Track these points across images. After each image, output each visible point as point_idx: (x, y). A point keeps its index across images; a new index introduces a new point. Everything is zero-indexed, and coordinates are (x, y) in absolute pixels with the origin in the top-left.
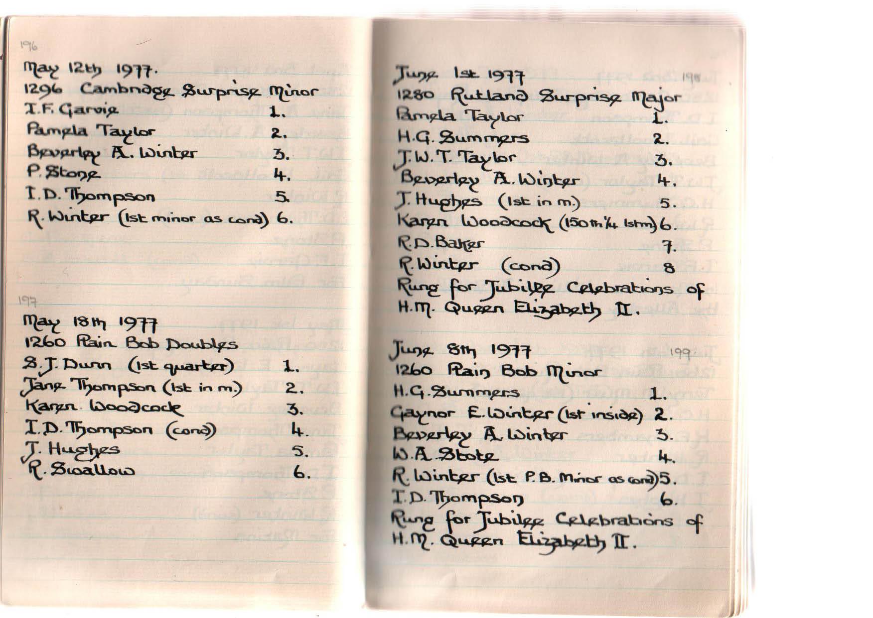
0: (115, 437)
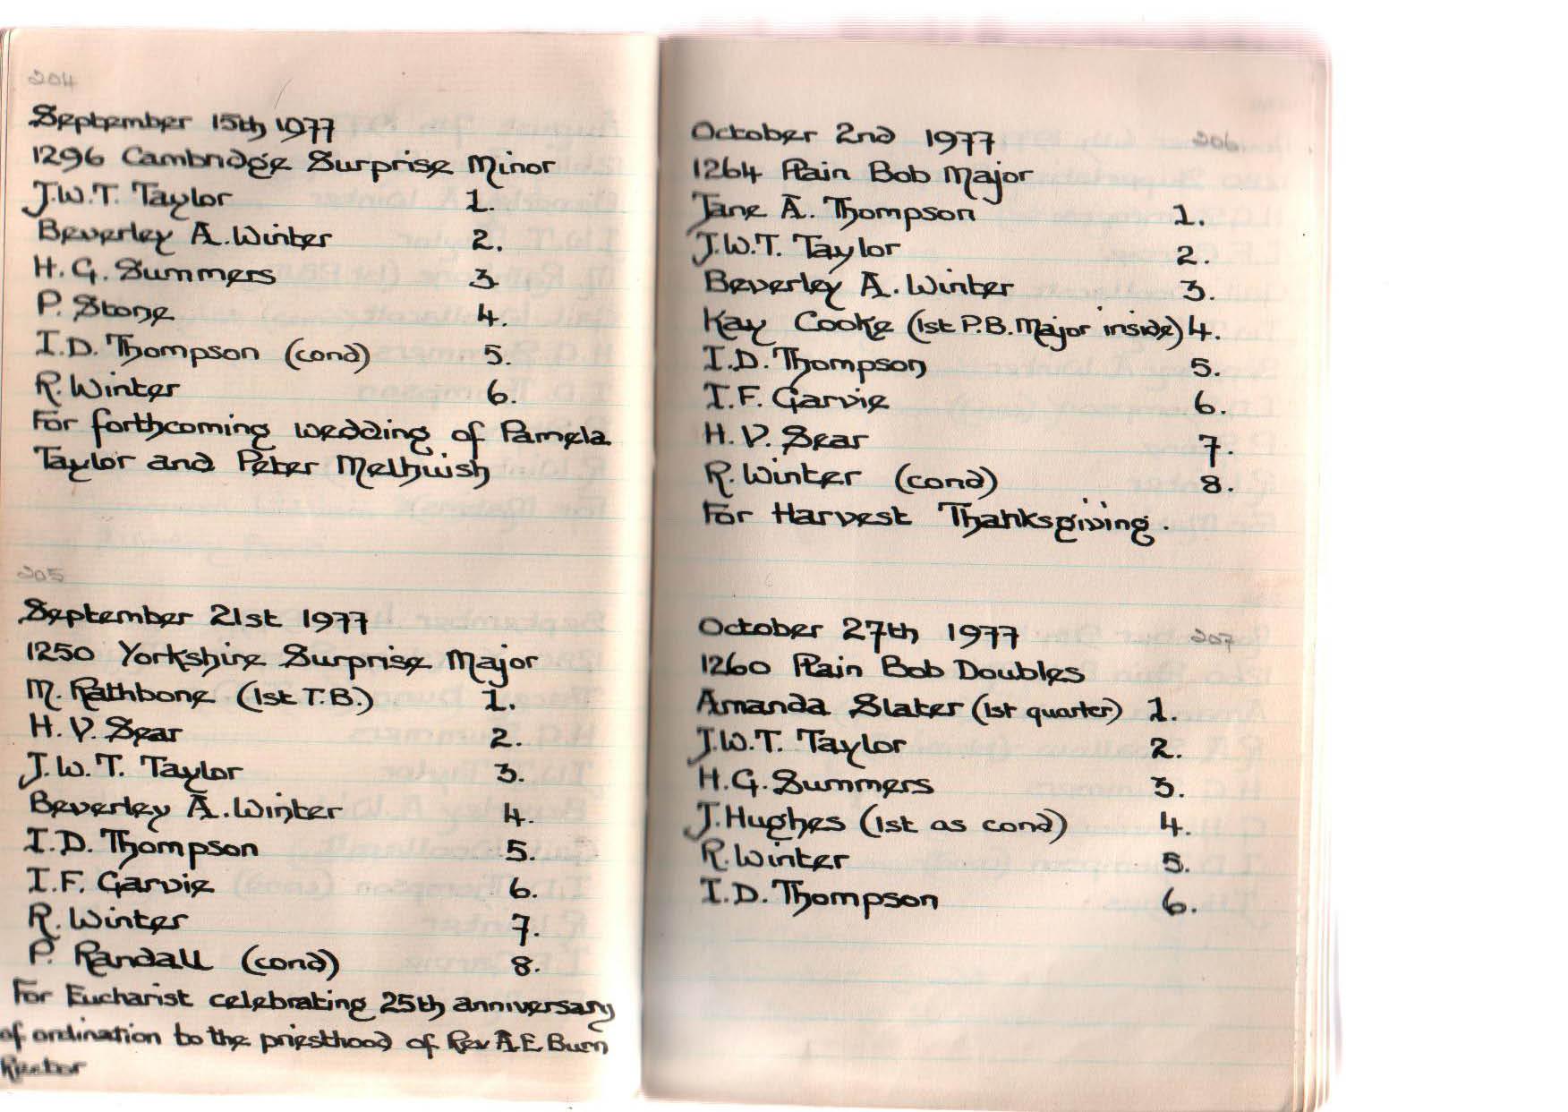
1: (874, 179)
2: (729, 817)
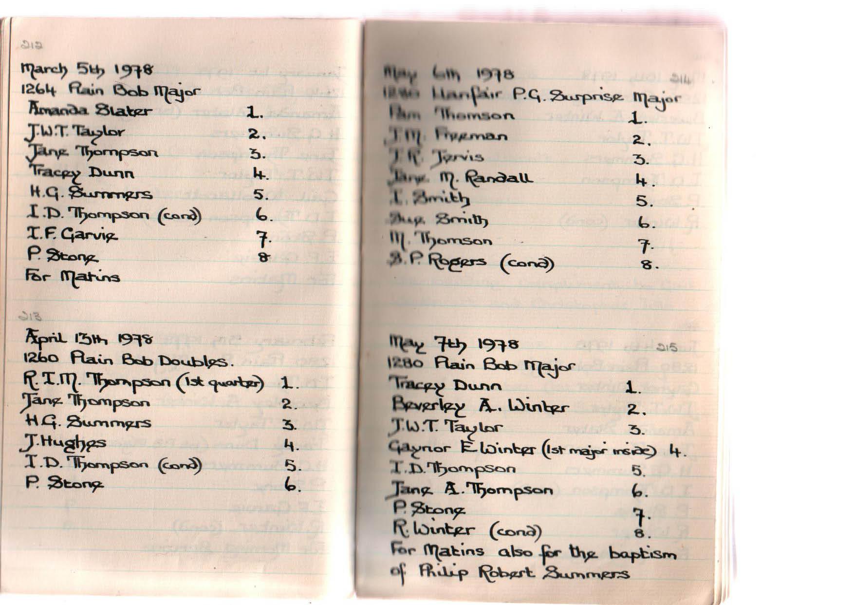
0: (114, 221)
1: (486, 368)
2: (43, 440)
